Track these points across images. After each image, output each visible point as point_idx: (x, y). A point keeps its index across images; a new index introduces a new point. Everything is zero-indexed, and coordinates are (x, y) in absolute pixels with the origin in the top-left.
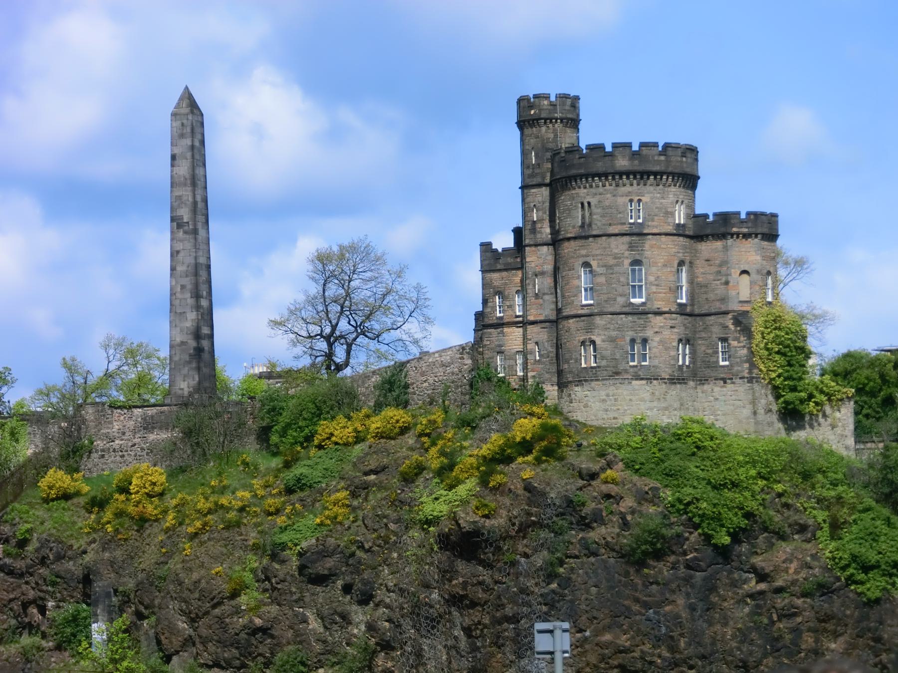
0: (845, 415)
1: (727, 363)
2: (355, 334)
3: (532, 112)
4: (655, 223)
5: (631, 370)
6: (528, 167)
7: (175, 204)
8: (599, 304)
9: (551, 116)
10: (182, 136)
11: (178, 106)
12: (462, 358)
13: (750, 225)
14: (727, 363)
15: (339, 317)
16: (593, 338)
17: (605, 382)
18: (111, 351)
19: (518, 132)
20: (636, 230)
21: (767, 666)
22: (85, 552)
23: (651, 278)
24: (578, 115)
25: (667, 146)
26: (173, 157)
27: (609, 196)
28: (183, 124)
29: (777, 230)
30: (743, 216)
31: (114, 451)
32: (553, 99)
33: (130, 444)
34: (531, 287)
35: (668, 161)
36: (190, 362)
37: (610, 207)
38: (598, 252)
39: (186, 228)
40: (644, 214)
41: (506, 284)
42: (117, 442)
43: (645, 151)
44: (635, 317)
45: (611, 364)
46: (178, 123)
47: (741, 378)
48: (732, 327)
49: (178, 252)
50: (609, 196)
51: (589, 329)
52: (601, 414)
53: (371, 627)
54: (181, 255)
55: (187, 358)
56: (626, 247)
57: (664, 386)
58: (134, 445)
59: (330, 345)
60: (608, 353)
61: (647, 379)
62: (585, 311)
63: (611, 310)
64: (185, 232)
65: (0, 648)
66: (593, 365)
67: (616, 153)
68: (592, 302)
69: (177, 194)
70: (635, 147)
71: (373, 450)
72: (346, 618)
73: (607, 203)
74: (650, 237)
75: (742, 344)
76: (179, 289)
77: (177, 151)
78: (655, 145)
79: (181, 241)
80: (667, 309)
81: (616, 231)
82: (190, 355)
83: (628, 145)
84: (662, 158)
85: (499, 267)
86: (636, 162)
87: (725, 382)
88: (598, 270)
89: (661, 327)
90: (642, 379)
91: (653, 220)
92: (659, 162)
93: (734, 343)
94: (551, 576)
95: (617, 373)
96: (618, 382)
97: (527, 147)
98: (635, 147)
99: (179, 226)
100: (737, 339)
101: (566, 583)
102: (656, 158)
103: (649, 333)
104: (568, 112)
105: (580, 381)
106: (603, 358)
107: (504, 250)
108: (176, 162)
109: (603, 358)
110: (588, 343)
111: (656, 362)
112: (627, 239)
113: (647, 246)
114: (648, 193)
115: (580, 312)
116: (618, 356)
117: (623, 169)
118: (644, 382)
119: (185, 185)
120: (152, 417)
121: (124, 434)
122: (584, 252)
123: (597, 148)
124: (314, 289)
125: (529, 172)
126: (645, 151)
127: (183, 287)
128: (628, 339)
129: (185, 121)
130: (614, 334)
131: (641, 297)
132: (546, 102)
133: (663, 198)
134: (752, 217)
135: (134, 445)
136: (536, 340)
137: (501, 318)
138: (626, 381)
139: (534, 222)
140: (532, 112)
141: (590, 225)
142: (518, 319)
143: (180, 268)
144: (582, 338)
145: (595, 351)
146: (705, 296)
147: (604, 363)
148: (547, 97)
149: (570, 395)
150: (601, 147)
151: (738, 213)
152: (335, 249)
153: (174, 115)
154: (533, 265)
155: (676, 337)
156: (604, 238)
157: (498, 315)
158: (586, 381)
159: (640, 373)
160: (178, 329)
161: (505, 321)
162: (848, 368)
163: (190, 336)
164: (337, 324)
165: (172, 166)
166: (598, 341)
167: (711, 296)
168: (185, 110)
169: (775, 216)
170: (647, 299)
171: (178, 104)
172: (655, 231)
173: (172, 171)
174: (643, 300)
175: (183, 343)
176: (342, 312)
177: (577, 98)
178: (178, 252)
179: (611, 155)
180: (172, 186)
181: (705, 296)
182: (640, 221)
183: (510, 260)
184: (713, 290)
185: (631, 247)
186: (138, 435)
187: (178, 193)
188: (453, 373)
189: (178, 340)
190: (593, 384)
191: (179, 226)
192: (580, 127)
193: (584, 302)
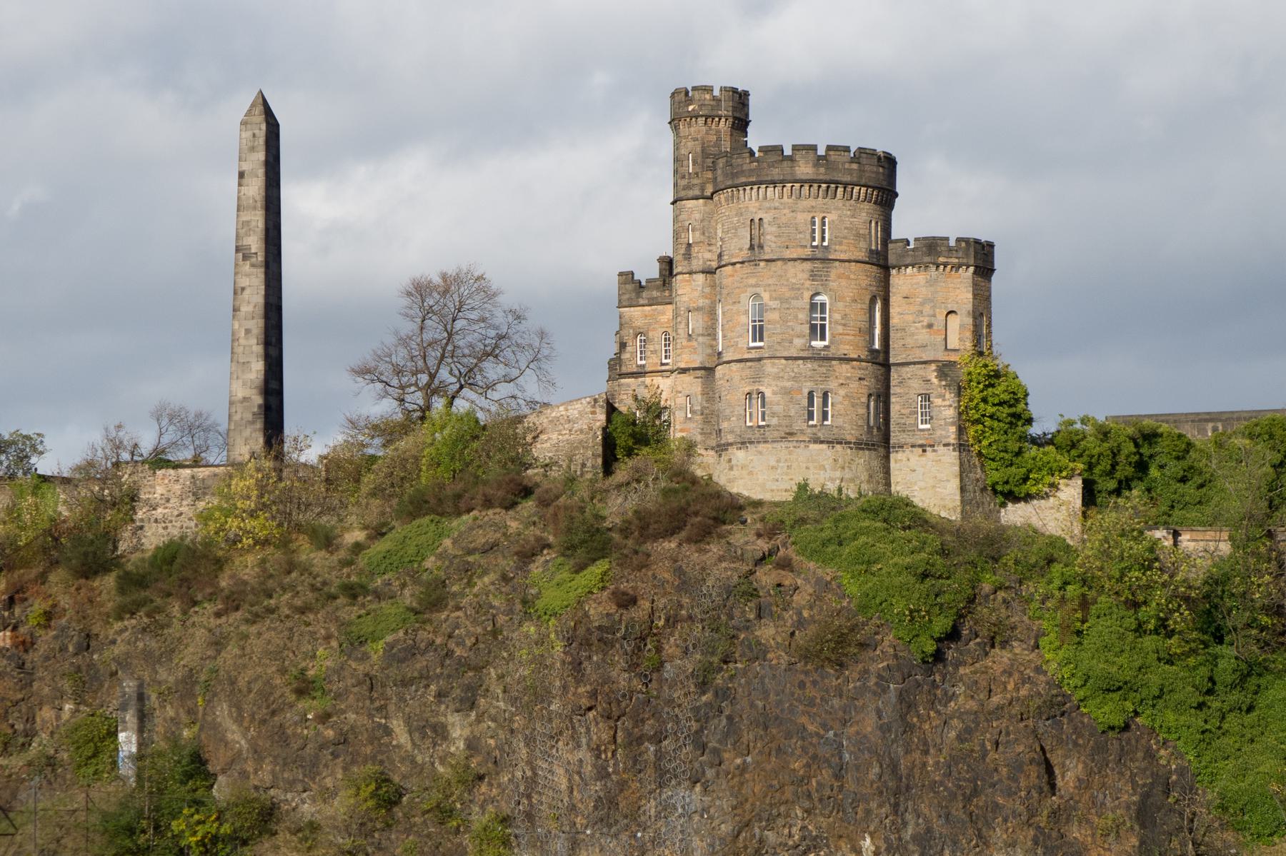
0: (1071, 492)
1: (928, 426)
2: (458, 386)
3: (691, 108)
4: (844, 248)
5: (809, 431)
6: (683, 177)
7: (242, 232)
8: (769, 347)
9: (715, 113)
10: (252, 149)
11: (249, 113)
12: (593, 413)
13: (960, 254)
14: (928, 426)
15: (440, 363)
16: (762, 389)
17: (775, 445)
18: (165, 422)
19: (669, 136)
20: (819, 255)
21: (977, 806)
22: (114, 642)
23: (837, 316)
24: (747, 115)
25: (861, 150)
26: (241, 175)
27: (786, 211)
28: (254, 135)
29: (993, 263)
30: (952, 243)
31: (156, 521)
32: (716, 93)
33: (176, 513)
34: (683, 326)
35: (861, 171)
36: (253, 422)
37: (787, 226)
38: (770, 281)
39: (254, 260)
40: (831, 235)
41: (650, 324)
42: (160, 510)
43: (834, 156)
44: (815, 365)
45: (784, 422)
46: (249, 134)
47: (945, 445)
48: (935, 381)
49: (243, 289)
50: (786, 211)
51: (756, 379)
52: (770, 485)
53: (472, 745)
54: (247, 292)
55: (249, 416)
56: (806, 275)
57: (849, 451)
58: (181, 514)
59: (428, 399)
60: (779, 409)
61: (828, 442)
62: (753, 355)
63: (786, 354)
64: (253, 265)
65: (1283, 694)
66: (761, 423)
67: (797, 157)
68: (761, 344)
69: (245, 219)
70: (821, 151)
71: (479, 522)
72: (441, 732)
73: (784, 220)
74: (837, 263)
75: (947, 403)
76: (243, 334)
77: (246, 167)
78: (847, 149)
79: (247, 275)
80: (856, 356)
81: (795, 256)
82: (254, 414)
83: (813, 148)
84: (855, 166)
85: (641, 302)
86: (822, 170)
87: (924, 451)
88: (771, 303)
89: (848, 378)
90: (822, 442)
91: (841, 244)
92: (850, 171)
93: (938, 402)
94: (703, 686)
95: (791, 434)
96: (790, 445)
97: (683, 152)
98: (821, 151)
99: (245, 258)
100: (943, 397)
101: (723, 694)
102: (847, 166)
103: (832, 385)
104: (738, 107)
105: (743, 443)
106: (773, 414)
107: (648, 281)
108: (245, 181)
109: (773, 414)
110: (755, 396)
111: (840, 421)
112: (808, 265)
113: (833, 275)
114: (837, 209)
115: (746, 356)
116: (792, 413)
117: (803, 177)
118: (824, 446)
119: (255, 208)
120: (203, 480)
121: (168, 500)
122: (752, 281)
123: (774, 150)
124: (409, 327)
125: (683, 182)
126: (834, 156)
127: (248, 331)
128: (806, 392)
129: (257, 132)
130: (789, 384)
131: (823, 338)
132: (708, 97)
133: (853, 216)
134: (963, 244)
135: (181, 514)
136: (688, 392)
137: (643, 366)
138: (802, 445)
139: (689, 245)
140: (691, 108)
141: (761, 247)
142: (664, 368)
143: (245, 309)
144: (747, 389)
145: (763, 406)
146: (902, 342)
147: (774, 421)
148: (708, 89)
149: (730, 460)
150: (779, 149)
151: (947, 239)
152: (437, 280)
153: (244, 123)
154: (685, 299)
155: (866, 391)
156: (779, 263)
157: (639, 362)
158: (751, 443)
159: (820, 434)
160: (240, 382)
161: (648, 369)
162: (1068, 442)
163: (254, 391)
164: (437, 371)
165: (240, 185)
166: (768, 393)
167: (910, 341)
168: (259, 119)
169: (991, 245)
170: (831, 342)
171: (250, 111)
172: (843, 257)
173: (239, 192)
174: (826, 343)
175: (245, 399)
176: (443, 357)
177: (746, 94)
178: (243, 289)
179: (791, 159)
180: (238, 210)
181: (902, 342)
182: (825, 244)
183: (655, 294)
184: (913, 334)
185: (813, 276)
186: (185, 503)
187: (246, 217)
188: (581, 431)
189: (240, 395)
190: (761, 447)
191: (245, 258)
192: (749, 129)
193: (752, 344)
